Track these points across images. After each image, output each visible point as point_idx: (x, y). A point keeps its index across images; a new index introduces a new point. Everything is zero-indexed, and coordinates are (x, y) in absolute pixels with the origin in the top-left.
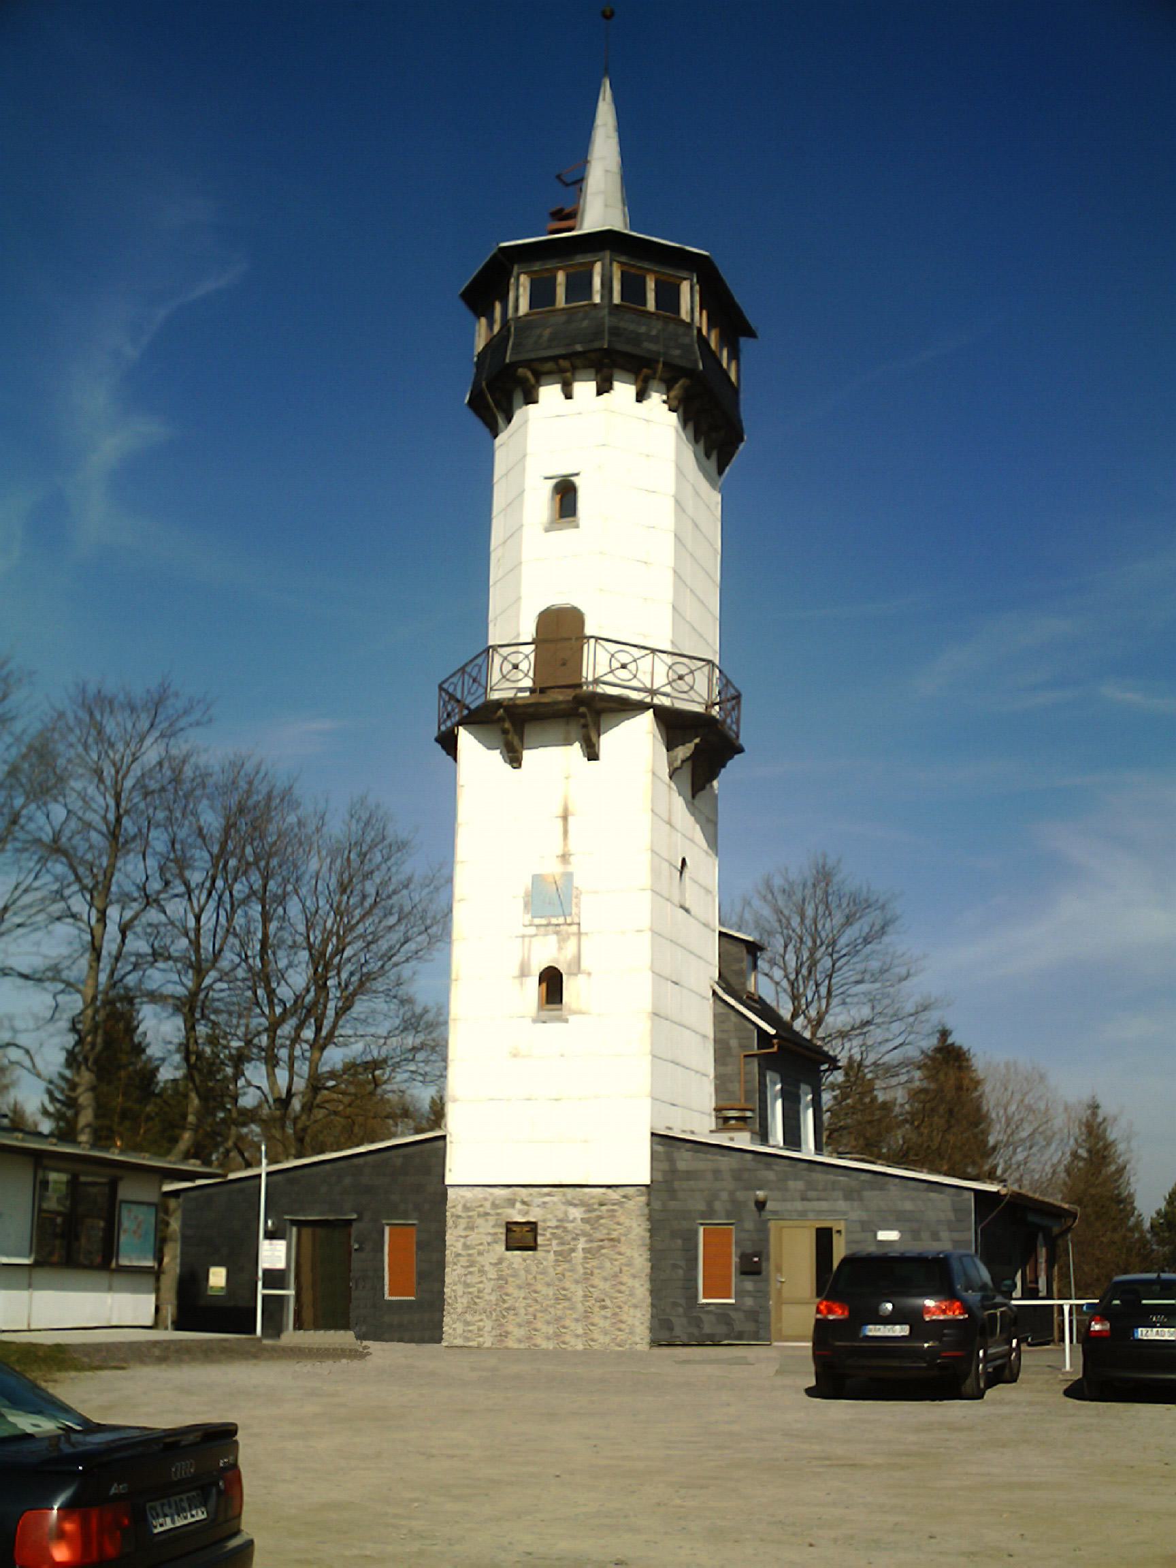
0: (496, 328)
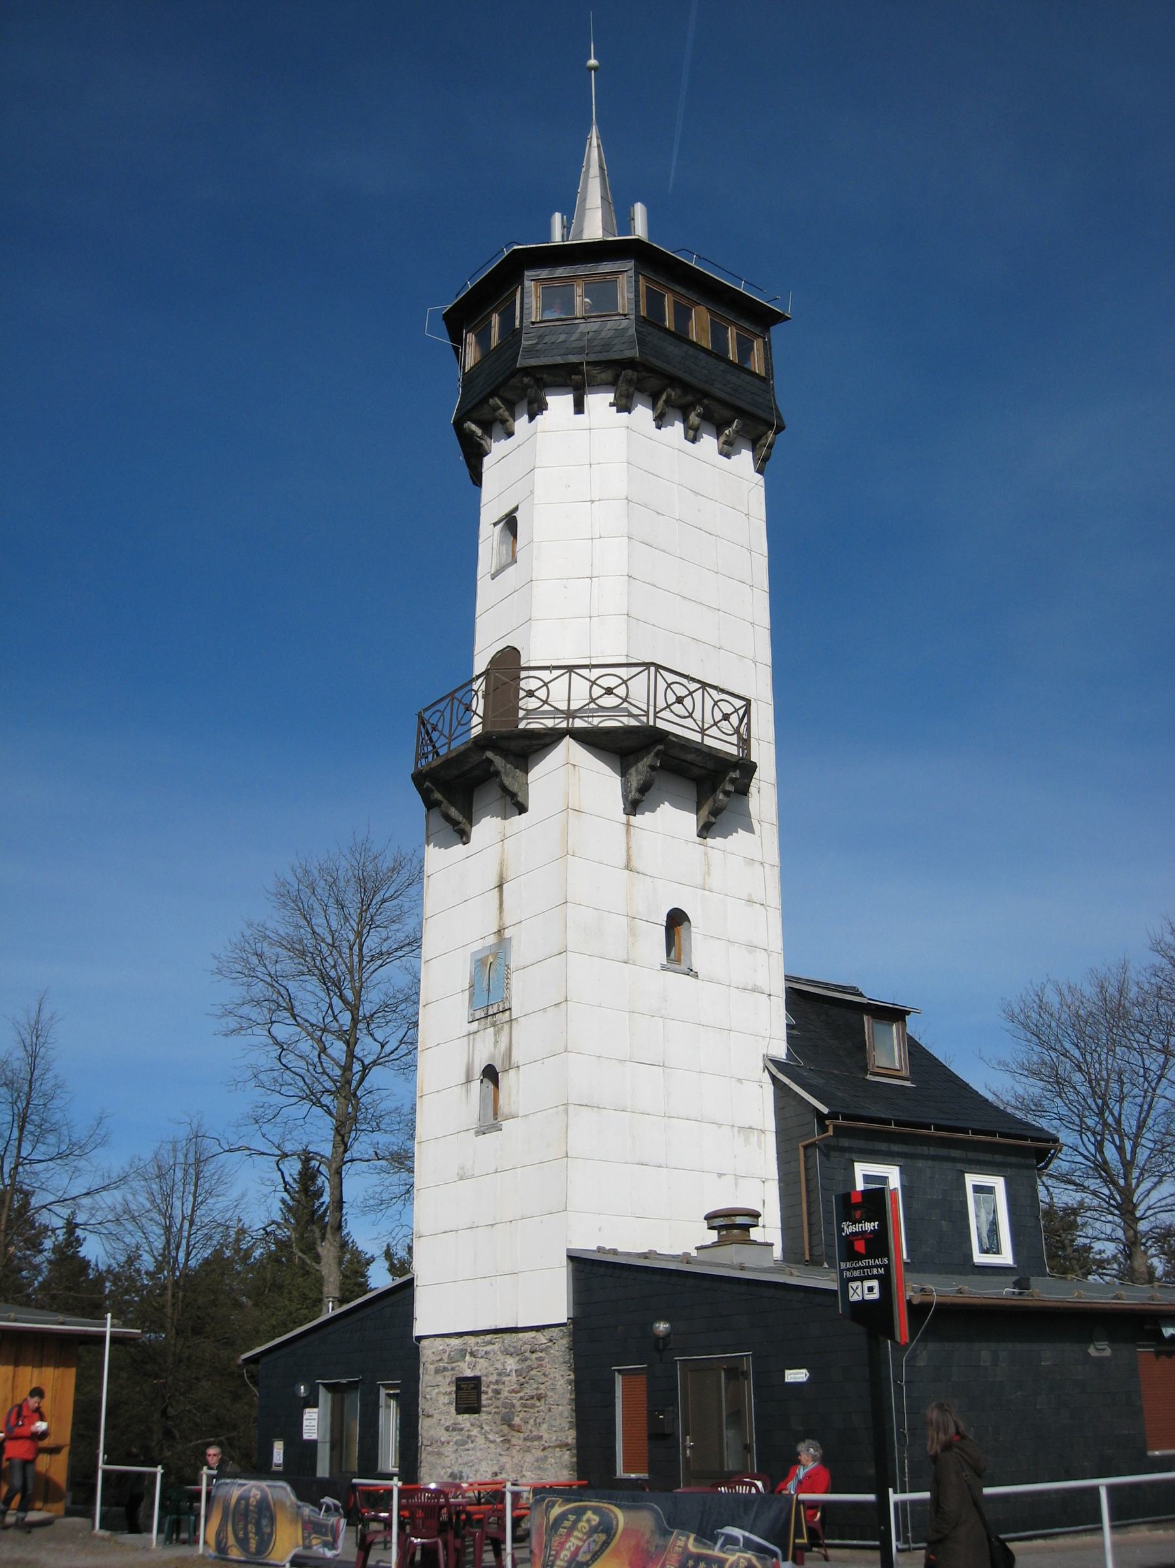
0: (495, 340)
